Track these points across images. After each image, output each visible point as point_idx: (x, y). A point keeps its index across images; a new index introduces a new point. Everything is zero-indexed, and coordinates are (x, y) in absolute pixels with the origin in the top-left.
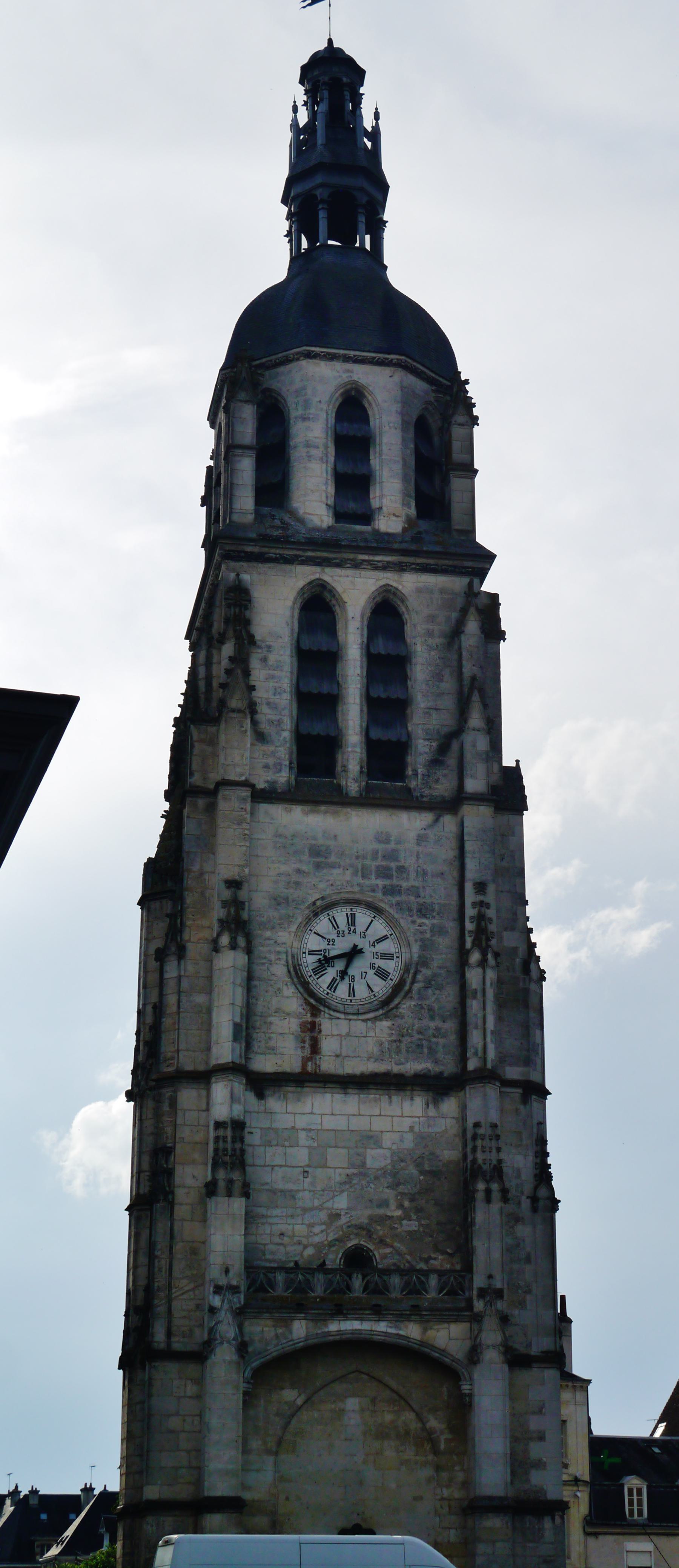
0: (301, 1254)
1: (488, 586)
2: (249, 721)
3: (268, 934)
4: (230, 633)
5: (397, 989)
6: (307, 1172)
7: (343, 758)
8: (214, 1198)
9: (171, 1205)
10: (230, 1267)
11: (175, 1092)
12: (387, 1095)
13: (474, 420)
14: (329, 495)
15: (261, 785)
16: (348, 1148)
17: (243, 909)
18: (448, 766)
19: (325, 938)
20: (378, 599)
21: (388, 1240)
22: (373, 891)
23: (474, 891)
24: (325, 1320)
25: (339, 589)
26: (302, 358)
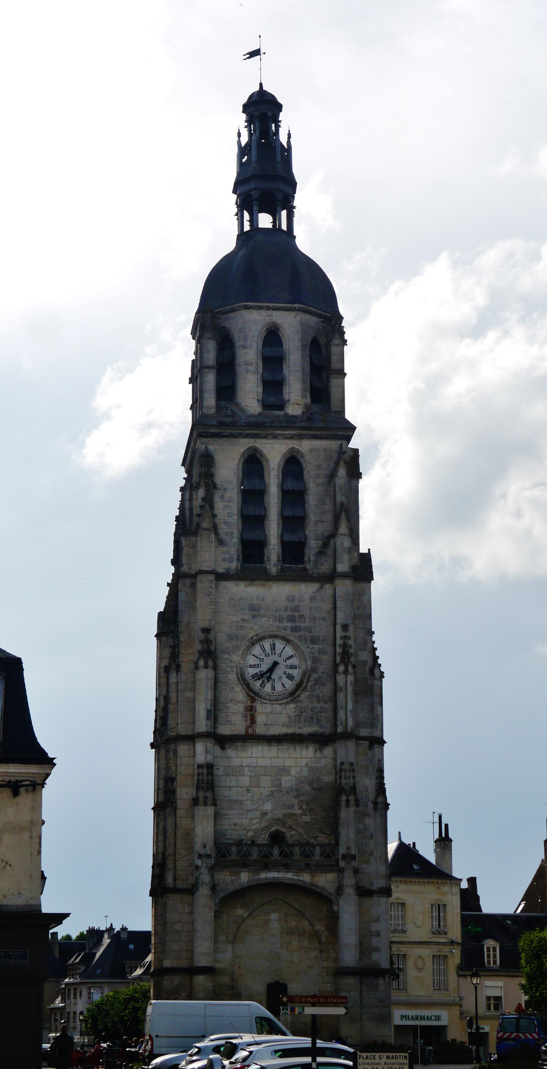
0: (246, 836)
1: (352, 445)
2: (213, 535)
3: (226, 656)
4: (202, 483)
5: (299, 686)
6: (249, 790)
7: (267, 553)
8: (197, 807)
9: (175, 809)
10: (207, 844)
11: (176, 746)
12: (293, 746)
13: (344, 342)
14: (259, 393)
15: (221, 570)
16: (272, 776)
17: (212, 644)
18: (328, 555)
19: (258, 658)
20: (288, 456)
21: (294, 827)
22: (285, 630)
23: (342, 630)
24: (258, 872)
25: (265, 452)
26: (242, 309)
